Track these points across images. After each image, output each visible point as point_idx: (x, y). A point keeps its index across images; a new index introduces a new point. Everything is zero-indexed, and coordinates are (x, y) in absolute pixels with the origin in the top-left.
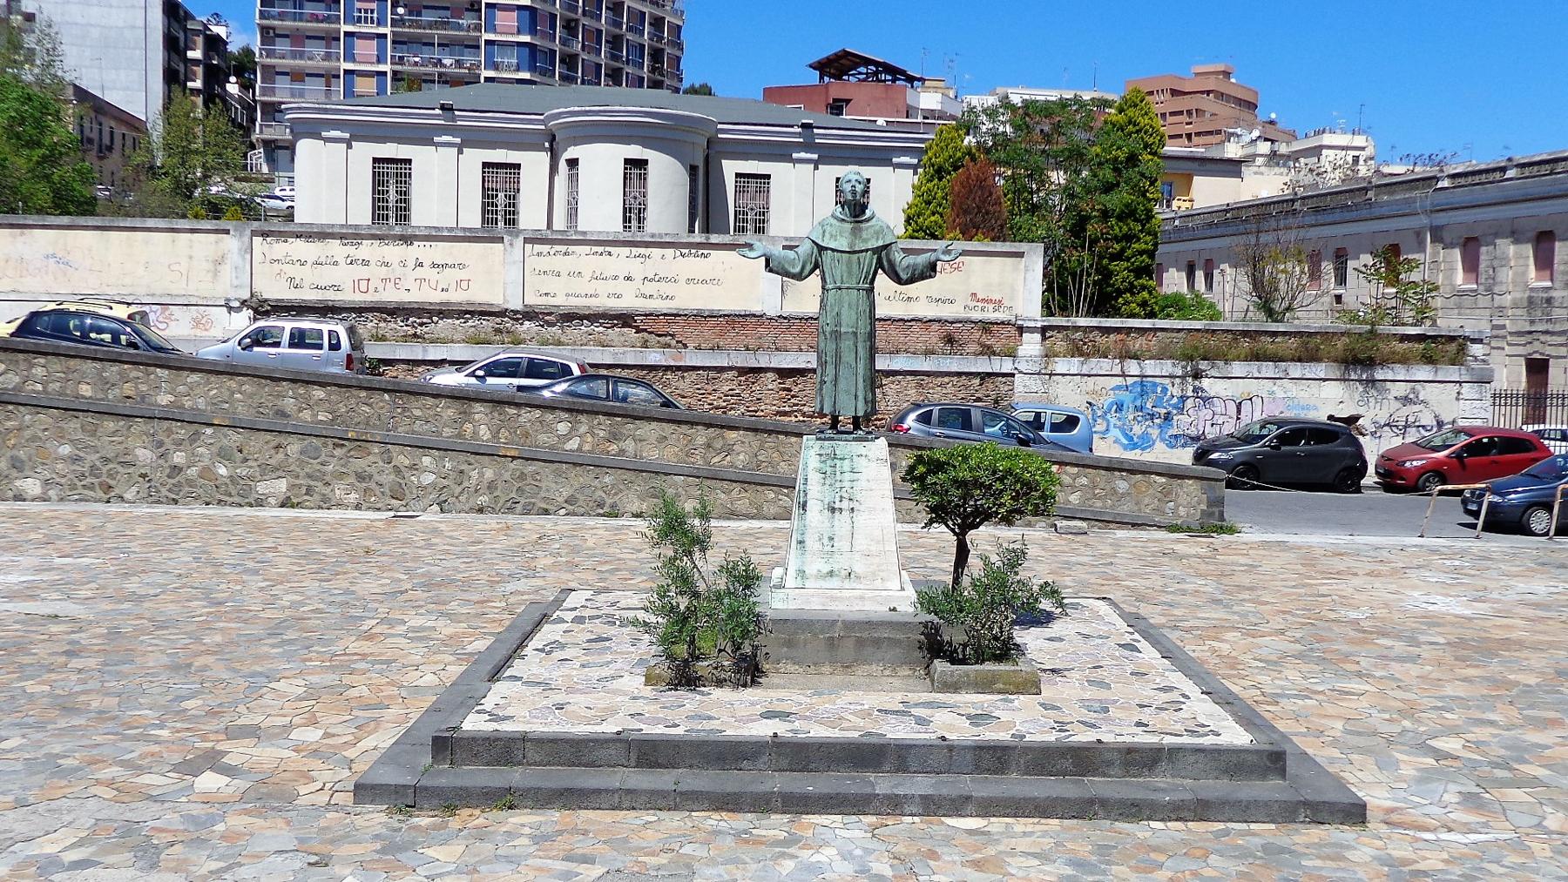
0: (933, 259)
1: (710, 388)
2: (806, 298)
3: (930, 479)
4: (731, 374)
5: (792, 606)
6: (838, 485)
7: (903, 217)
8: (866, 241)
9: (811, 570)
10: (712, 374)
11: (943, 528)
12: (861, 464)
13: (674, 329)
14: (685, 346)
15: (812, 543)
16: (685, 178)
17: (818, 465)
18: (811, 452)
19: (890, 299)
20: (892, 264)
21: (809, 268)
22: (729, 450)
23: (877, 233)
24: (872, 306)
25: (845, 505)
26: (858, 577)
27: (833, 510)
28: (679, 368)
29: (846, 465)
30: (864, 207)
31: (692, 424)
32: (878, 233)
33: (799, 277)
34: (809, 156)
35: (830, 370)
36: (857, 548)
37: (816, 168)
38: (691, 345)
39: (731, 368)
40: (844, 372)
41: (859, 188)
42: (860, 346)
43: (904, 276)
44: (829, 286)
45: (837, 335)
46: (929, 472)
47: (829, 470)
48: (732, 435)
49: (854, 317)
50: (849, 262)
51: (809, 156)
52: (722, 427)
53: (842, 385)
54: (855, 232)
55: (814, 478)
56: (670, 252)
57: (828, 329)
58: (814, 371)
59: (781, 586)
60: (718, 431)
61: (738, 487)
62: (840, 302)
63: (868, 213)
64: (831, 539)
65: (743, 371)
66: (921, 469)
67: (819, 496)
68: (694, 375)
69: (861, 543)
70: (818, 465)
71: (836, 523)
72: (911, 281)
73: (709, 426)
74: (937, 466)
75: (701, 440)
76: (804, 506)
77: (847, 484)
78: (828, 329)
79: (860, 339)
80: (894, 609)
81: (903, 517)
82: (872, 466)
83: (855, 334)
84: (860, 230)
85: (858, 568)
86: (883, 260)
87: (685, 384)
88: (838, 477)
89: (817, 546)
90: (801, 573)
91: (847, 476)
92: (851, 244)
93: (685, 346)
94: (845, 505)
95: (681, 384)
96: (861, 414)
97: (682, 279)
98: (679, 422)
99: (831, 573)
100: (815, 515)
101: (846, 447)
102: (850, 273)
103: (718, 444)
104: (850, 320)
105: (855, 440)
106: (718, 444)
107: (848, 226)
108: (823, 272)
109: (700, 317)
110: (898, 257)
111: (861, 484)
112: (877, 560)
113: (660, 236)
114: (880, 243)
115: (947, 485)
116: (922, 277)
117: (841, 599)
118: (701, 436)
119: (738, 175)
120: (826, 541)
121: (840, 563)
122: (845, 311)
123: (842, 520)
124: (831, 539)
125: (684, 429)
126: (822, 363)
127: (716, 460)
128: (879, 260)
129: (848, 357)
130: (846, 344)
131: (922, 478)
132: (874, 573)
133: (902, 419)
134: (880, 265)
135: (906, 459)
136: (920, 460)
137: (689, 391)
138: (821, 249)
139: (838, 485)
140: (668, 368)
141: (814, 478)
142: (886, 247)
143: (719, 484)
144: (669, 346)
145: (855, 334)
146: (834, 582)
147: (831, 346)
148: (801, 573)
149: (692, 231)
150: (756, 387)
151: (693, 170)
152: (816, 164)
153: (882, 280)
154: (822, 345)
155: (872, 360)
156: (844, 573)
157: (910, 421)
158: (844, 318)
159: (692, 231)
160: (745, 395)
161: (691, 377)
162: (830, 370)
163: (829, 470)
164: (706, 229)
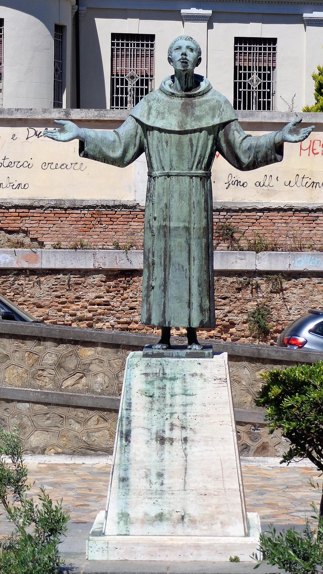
0: (278, 138)
1: (72, 295)
2: (128, 184)
3: (287, 402)
4: (98, 278)
5: (114, 556)
6: (168, 410)
7: (313, 86)
8: (199, 118)
9: (136, 513)
10: (74, 279)
11: (307, 462)
12: (195, 384)
13: (26, 225)
14: (42, 245)
15: (137, 481)
16: (47, 40)
17: (144, 386)
18: (136, 370)
19: (231, 186)
20: (230, 145)
21: (132, 152)
22: (83, 371)
23: (213, 109)
24: (208, 195)
25: (177, 434)
26: (193, 521)
27: (162, 440)
28: (33, 272)
29: (178, 386)
30: (199, 79)
31: (39, 339)
32: (214, 110)
33: (121, 162)
34: (201, 12)
35: (158, 272)
36: (191, 485)
37: (210, 27)
38: (48, 243)
39: (97, 271)
40: (173, 274)
41: (191, 56)
42: (194, 243)
43: (245, 160)
44: (156, 173)
45: (166, 231)
46: (285, 393)
47: (157, 393)
48: (88, 352)
49: (186, 209)
50: (179, 144)
51: (201, 12)
52: (75, 342)
53: (172, 290)
54: (187, 109)
55: (139, 403)
56: (22, 131)
57: (156, 224)
58: (137, 273)
59: (101, 534)
60: (71, 348)
61: (95, 416)
62: (169, 192)
63: (203, 85)
64: (160, 475)
65: (113, 274)
66: (276, 390)
67: (144, 423)
68: (51, 280)
69: (196, 480)
70: (144, 386)
71: (166, 456)
72: (253, 165)
73: (59, 341)
74: (296, 387)
75: (50, 359)
76: (127, 436)
77: (178, 409)
78: (156, 224)
79: (194, 234)
80: (236, 560)
81: (249, 445)
82: (210, 389)
83: (187, 229)
84: (193, 106)
85: (193, 511)
86: (220, 142)
87: (42, 291)
88: (168, 401)
89: (143, 484)
90: (124, 517)
91: (179, 400)
92: (182, 123)
93: (42, 245)
94: (177, 434)
95: (36, 291)
96: (195, 324)
97: (37, 163)
98: (24, 338)
99: (160, 517)
100: (141, 446)
101: (180, 365)
102: (180, 156)
103: (71, 364)
104: (183, 211)
105: (189, 356)
106: (71, 364)
107: (178, 102)
108: (149, 157)
109: (62, 209)
110: (237, 135)
111: (196, 409)
112: (214, 501)
113: (10, 111)
114: (217, 121)
115: (306, 408)
116: (267, 161)
117: (172, 548)
118: (50, 353)
119: (114, 36)
120: (154, 478)
121: (171, 505)
122: (175, 204)
123: (173, 453)
124: (160, 475)
125: (30, 345)
126: (150, 265)
127: (69, 382)
128: (216, 141)
129: (179, 257)
130: (177, 242)
131: (277, 402)
132: (212, 517)
133: (297, 330)
134: (217, 147)
135: (257, 376)
136: (275, 379)
137: (46, 300)
138: (147, 129)
139: (168, 410)
140: (20, 272)
141: (139, 403)
142: (224, 125)
143: (73, 412)
144: (21, 245)
145: (187, 229)
146: (165, 527)
147: (159, 245)
148: (124, 517)
149: (57, 104)
150: (128, 294)
151: (58, 31)
152: (210, 22)
153: (220, 164)
154: (149, 244)
155: (209, 258)
156: (176, 516)
157: (305, 335)
158: (175, 212)
159: (57, 104)
160: (115, 303)
161: (48, 281)
162: (158, 272)
163: (157, 393)
164: (77, 104)
